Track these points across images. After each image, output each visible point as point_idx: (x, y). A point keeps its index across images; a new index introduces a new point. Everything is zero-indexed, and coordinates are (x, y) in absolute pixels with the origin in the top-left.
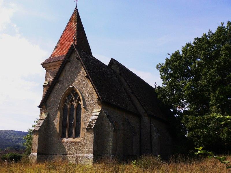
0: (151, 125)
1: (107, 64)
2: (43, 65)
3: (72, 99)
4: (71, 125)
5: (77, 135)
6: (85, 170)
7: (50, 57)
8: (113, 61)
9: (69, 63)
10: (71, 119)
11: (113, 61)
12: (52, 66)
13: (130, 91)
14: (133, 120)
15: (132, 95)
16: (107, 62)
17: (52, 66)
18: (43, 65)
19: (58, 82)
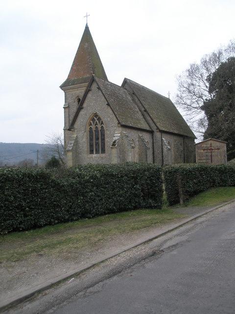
0: (162, 140)
1: (120, 85)
2: (61, 87)
3: (96, 122)
4: (97, 144)
5: (103, 151)
6: (234, 311)
7: (67, 79)
8: (126, 81)
9: (90, 92)
10: (97, 139)
11: (126, 81)
12: (71, 88)
13: (143, 109)
14: (147, 137)
15: (145, 113)
16: (120, 83)
17: (71, 88)
18: (61, 87)
19: (83, 108)
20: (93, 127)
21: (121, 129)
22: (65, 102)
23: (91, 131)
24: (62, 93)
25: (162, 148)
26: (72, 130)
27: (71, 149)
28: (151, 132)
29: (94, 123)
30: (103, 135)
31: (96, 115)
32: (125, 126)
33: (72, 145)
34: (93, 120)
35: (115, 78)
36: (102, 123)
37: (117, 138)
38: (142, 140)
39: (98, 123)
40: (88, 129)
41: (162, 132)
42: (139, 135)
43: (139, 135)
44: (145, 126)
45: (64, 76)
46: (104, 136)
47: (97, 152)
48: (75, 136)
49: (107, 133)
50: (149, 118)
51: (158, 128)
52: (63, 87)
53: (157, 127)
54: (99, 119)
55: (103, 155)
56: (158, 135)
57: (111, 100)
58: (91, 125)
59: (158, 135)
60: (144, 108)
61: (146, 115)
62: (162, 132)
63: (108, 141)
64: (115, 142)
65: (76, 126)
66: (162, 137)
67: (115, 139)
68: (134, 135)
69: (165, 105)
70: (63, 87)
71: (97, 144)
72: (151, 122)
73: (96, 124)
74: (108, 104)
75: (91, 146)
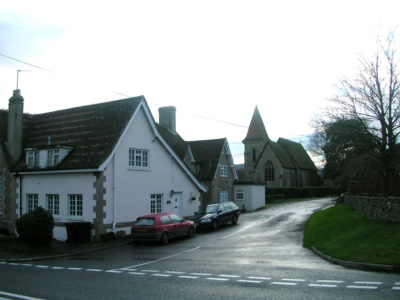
0: (301, 173)
4: (270, 176)
5: (273, 180)
14: (293, 172)
20: (268, 167)
21: (283, 169)
22: (245, 150)
23: (266, 169)
24: (243, 145)
25: (301, 178)
26: (256, 168)
27: (256, 178)
28: (295, 169)
29: (268, 165)
30: (273, 171)
31: (269, 161)
32: (285, 168)
33: (256, 176)
34: (268, 164)
35: (274, 137)
36: (273, 165)
37: (282, 174)
38: (291, 174)
39: (270, 165)
40: (265, 168)
41: (301, 169)
42: (290, 171)
43: (290, 171)
44: (292, 166)
45: (244, 135)
46: (274, 172)
47: (270, 180)
48: (258, 171)
49: (275, 170)
50: (294, 161)
51: (299, 167)
52: (243, 142)
53: (298, 166)
54: (271, 163)
55: (274, 182)
56: (299, 171)
57: (278, 154)
58: (266, 166)
59: (299, 171)
60: (291, 155)
61: (292, 159)
62: (301, 169)
63: (277, 175)
64: (281, 175)
65: (257, 166)
66: (301, 172)
67: (280, 174)
68: (288, 171)
69: (298, 147)
70: (243, 142)
71: (270, 176)
72: (295, 163)
73: (269, 165)
74: (277, 156)
75: (266, 177)
